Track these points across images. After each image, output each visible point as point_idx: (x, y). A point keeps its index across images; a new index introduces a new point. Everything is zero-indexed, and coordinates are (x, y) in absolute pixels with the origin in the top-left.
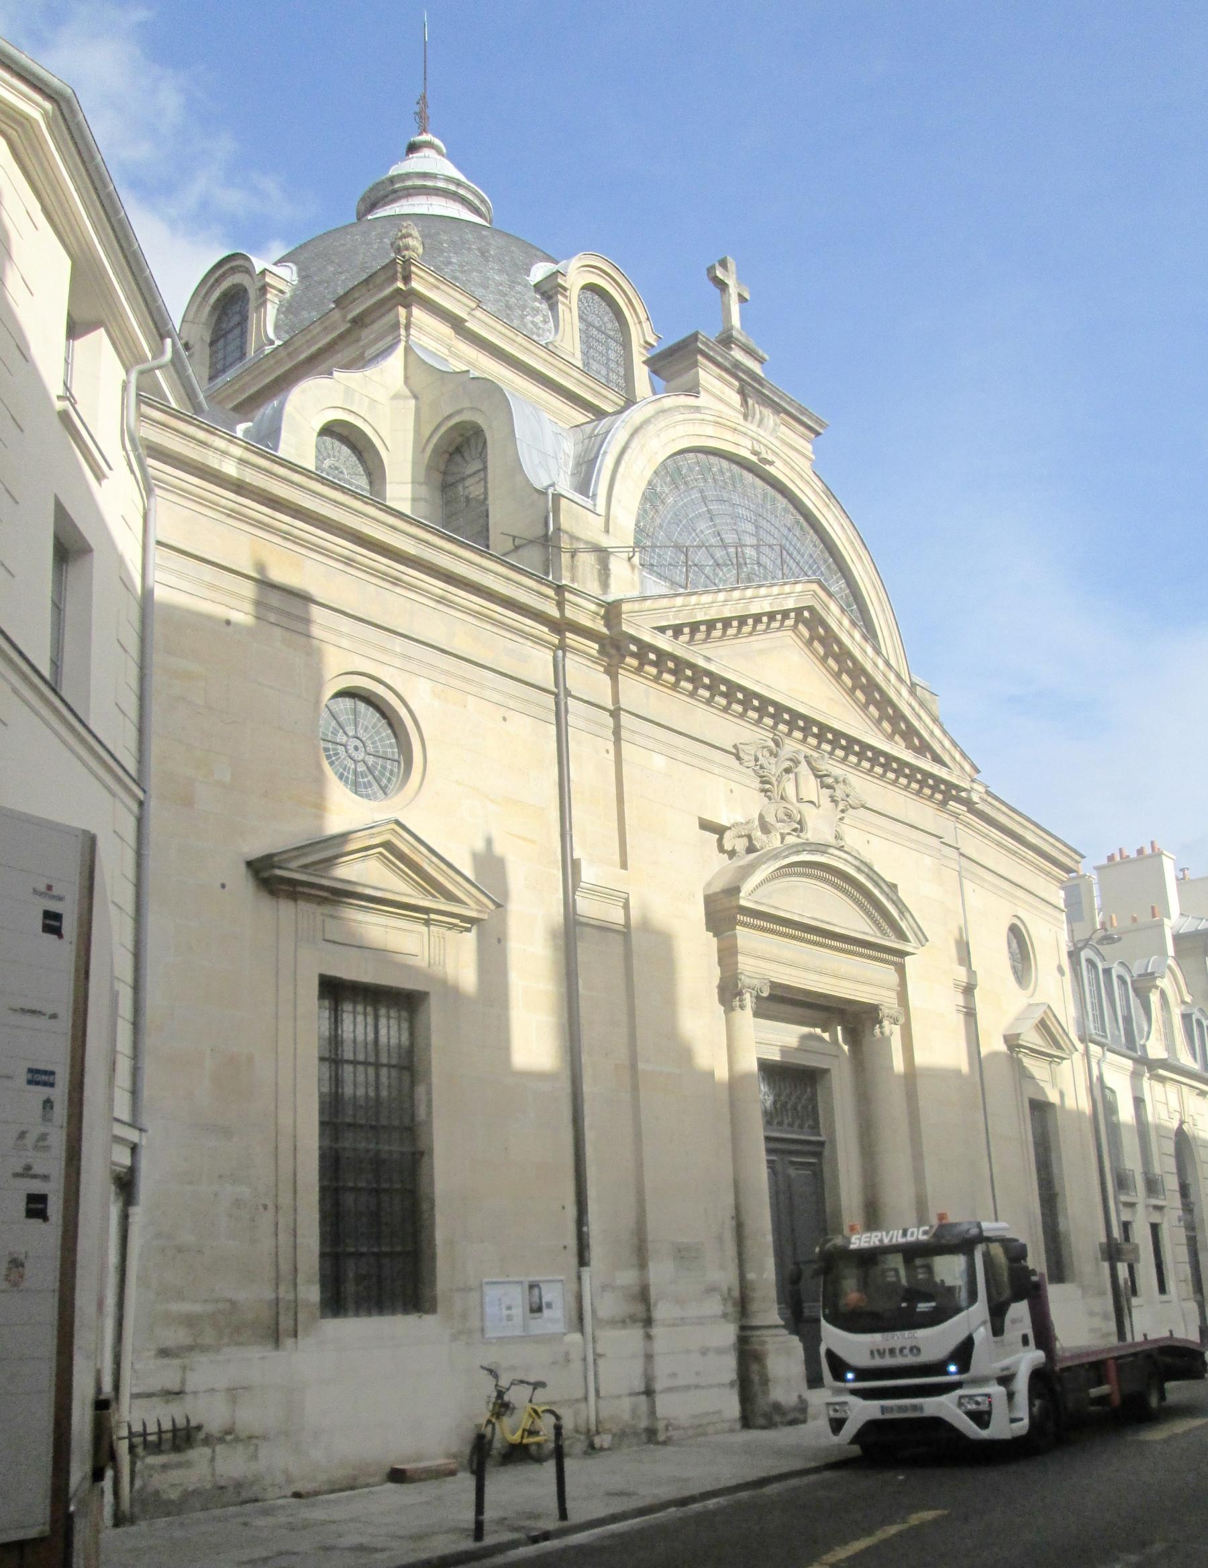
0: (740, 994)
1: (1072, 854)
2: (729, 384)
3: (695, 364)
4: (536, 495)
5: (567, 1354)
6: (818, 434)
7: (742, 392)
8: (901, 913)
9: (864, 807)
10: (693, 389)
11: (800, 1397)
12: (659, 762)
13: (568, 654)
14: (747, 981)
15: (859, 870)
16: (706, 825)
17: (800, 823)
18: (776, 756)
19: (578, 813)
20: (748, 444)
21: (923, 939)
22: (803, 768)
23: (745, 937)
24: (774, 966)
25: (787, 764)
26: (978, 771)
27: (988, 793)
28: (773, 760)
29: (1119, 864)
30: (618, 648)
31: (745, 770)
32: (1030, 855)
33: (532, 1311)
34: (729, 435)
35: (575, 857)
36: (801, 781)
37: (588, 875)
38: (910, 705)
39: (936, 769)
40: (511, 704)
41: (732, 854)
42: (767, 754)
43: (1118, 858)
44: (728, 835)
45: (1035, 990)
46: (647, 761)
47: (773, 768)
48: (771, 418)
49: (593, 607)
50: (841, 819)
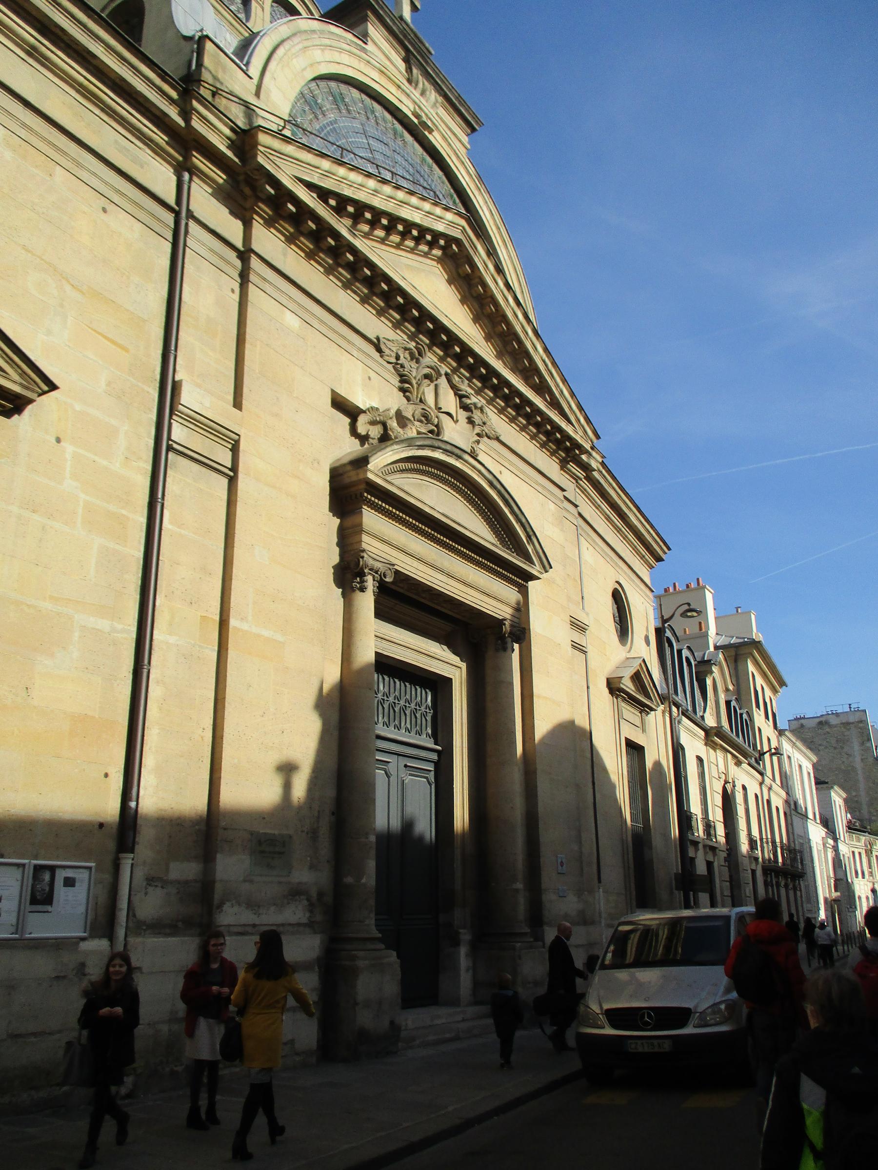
0: (362, 574)
1: (661, 544)
2: (397, 52)
3: (365, 19)
4: (183, 42)
5: (83, 965)
6: (473, 130)
7: (406, 60)
8: (529, 537)
9: (498, 439)
10: (364, 37)
11: (392, 1023)
12: (291, 321)
13: (195, 178)
14: (371, 562)
15: (491, 484)
16: (340, 404)
17: (437, 426)
18: (418, 361)
19: (186, 336)
20: (412, 107)
21: (546, 566)
22: (443, 381)
23: (371, 519)
24: (401, 556)
25: (427, 371)
26: (598, 437)
27: (603, 464)
28: (414, 364)
29: (672, 594)
30: (254, 188)
31: (385, 363)
32: (631, 536)
33: (34, 901)
34: (393, 89)
35: (177, 378)
36: (441, 391)
37: (189, 398)
38: (544, 361)
39: (563, 424)
40: (116, 198)
41: (363, 439)
42: (407, 356)
43: (671, 590)
44: (362, 420)
45: (631, 648)
46: (276, 316)
47: (414, 371)
48: (433, 95)
49: (227, 132)
50: (478, 442)
